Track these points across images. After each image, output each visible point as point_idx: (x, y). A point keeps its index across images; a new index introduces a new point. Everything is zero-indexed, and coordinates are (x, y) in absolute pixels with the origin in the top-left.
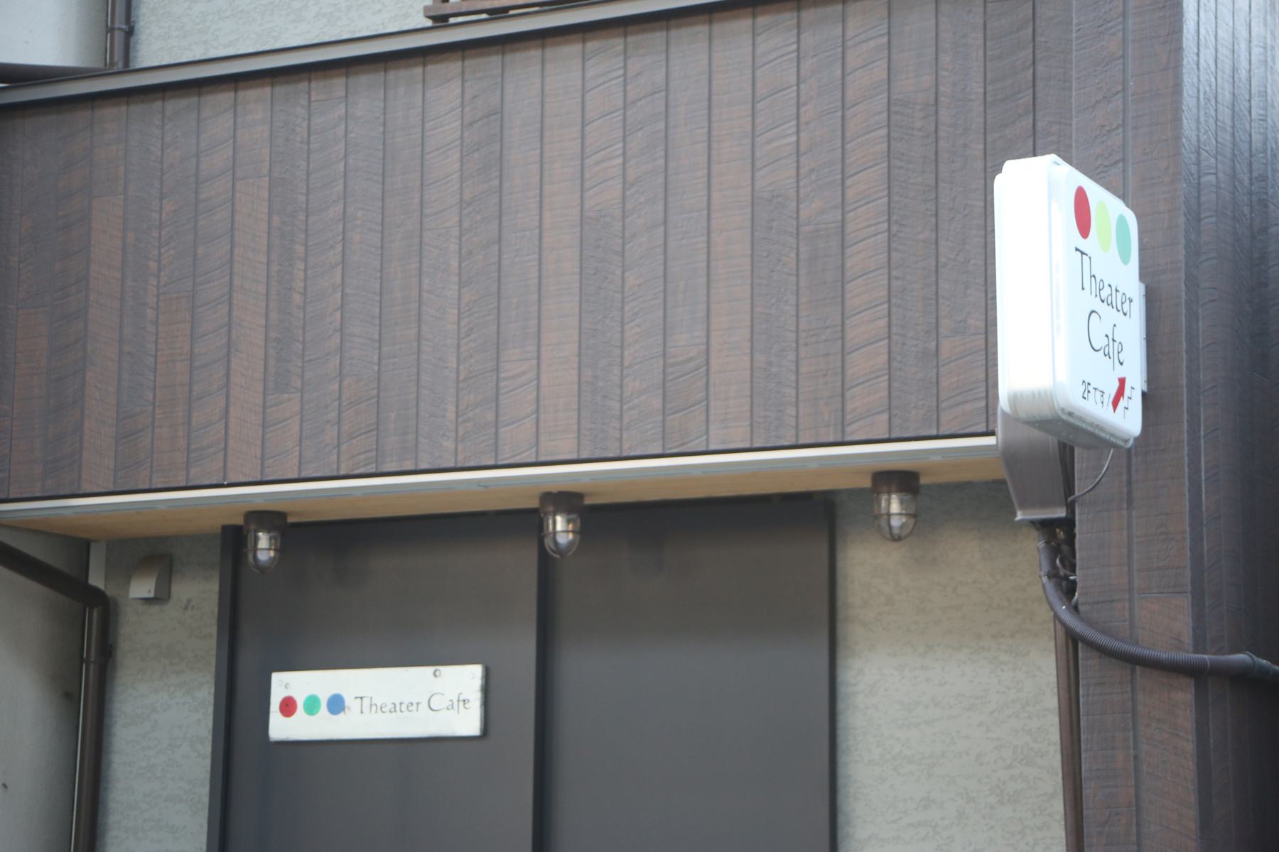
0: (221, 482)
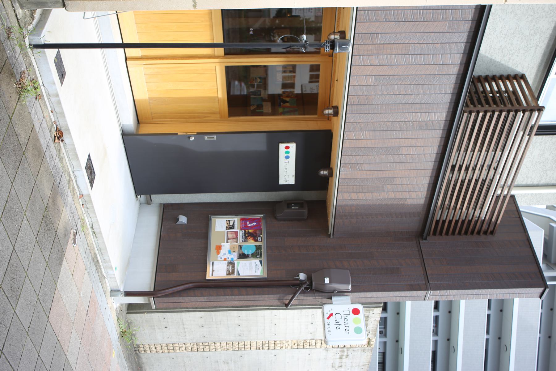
0: (352, 65)
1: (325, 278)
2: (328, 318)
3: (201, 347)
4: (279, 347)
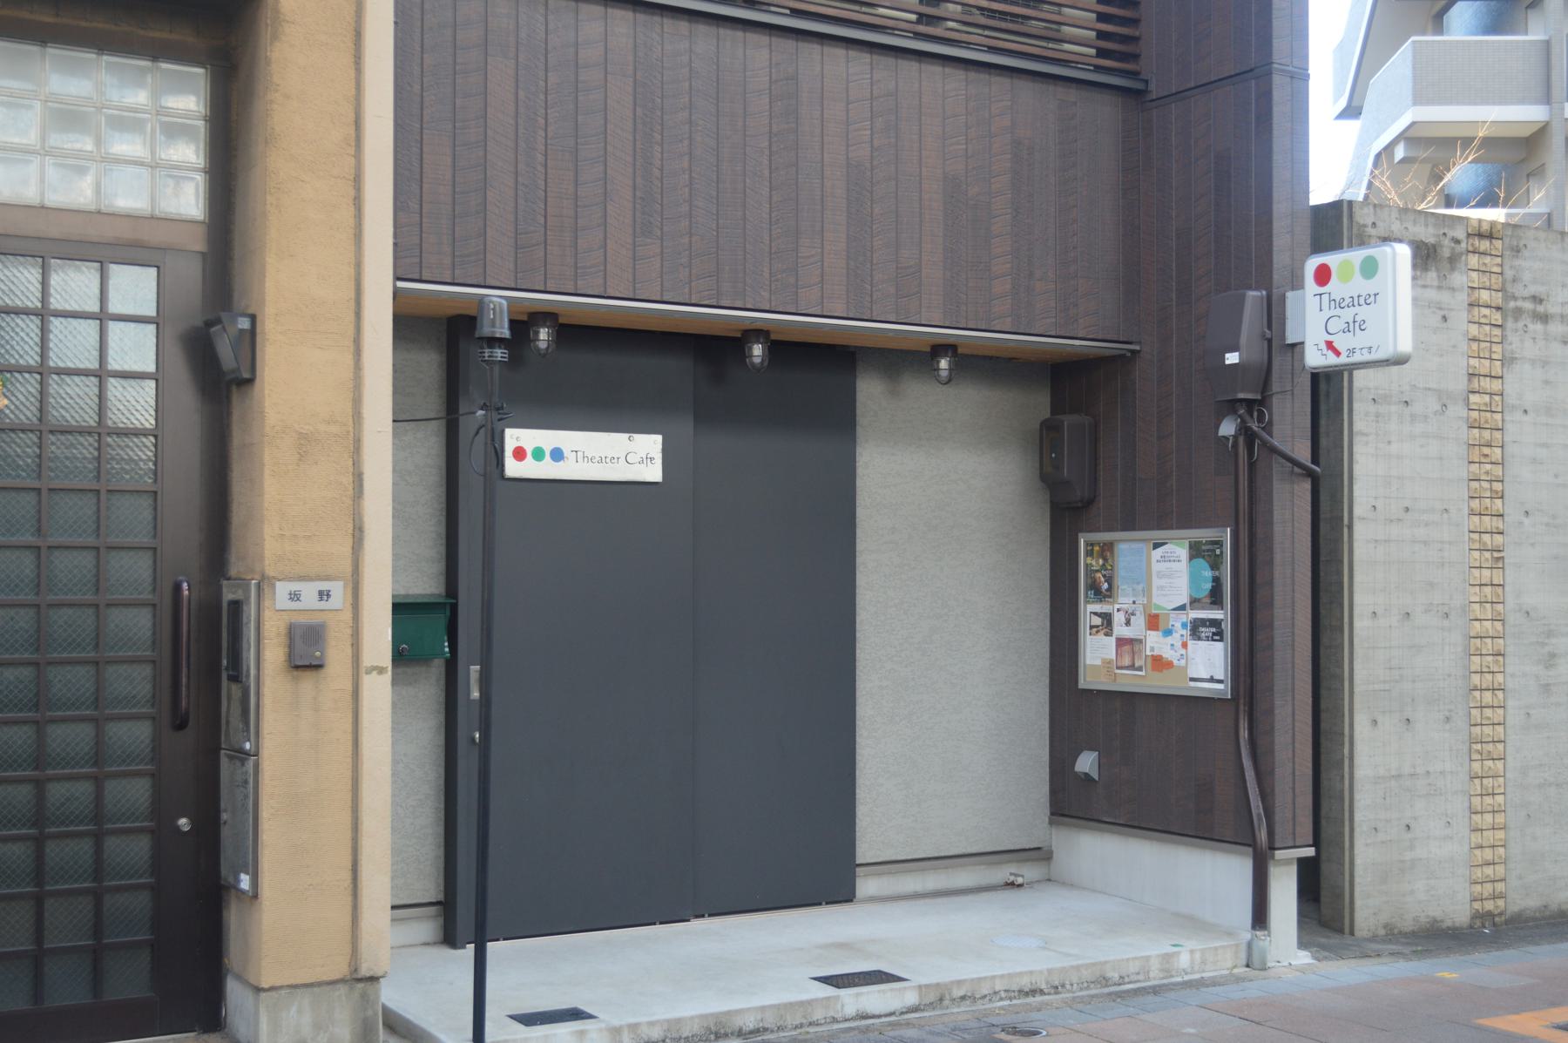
0: (603, 295)
1: (1227, 362)
2: (1338, 353)
3: (1488, 730)
4: (1496, 500)
